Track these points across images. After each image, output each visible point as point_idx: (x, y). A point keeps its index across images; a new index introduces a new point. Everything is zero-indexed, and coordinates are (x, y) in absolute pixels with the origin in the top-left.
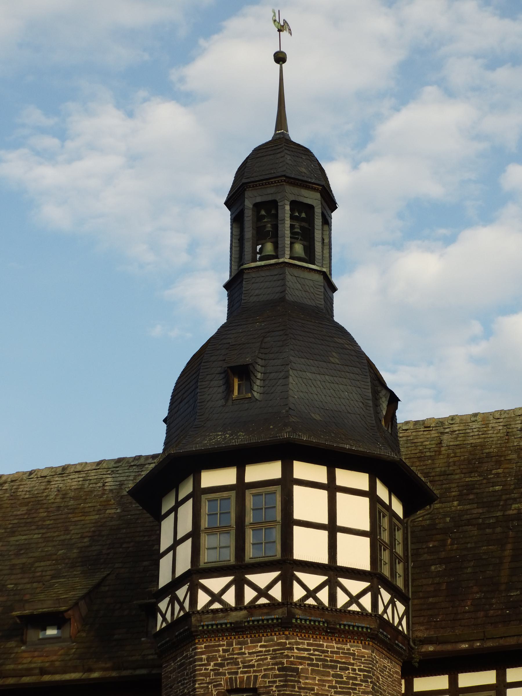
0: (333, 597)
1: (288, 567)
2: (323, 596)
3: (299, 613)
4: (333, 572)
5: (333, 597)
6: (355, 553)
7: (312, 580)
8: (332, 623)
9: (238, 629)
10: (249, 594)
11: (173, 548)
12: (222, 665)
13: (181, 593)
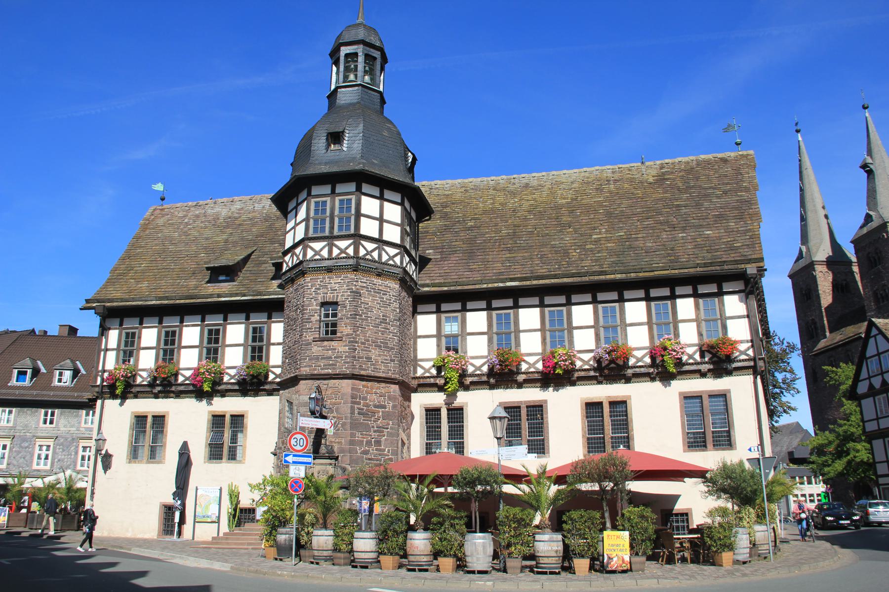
0: (380, 256)
1: (358, 237)
2: (375, 255)
3: (362, 263)
4: (380, 241)
5: (380, 256)
6: (393, 234)
7: (370, 246)
8: (381, 271)
9: (329, 270)
10: (336, 252)
11: (294, 228)
12: (319, 289)
13: (298, 250)
